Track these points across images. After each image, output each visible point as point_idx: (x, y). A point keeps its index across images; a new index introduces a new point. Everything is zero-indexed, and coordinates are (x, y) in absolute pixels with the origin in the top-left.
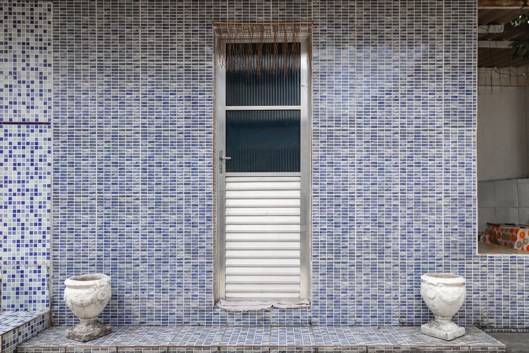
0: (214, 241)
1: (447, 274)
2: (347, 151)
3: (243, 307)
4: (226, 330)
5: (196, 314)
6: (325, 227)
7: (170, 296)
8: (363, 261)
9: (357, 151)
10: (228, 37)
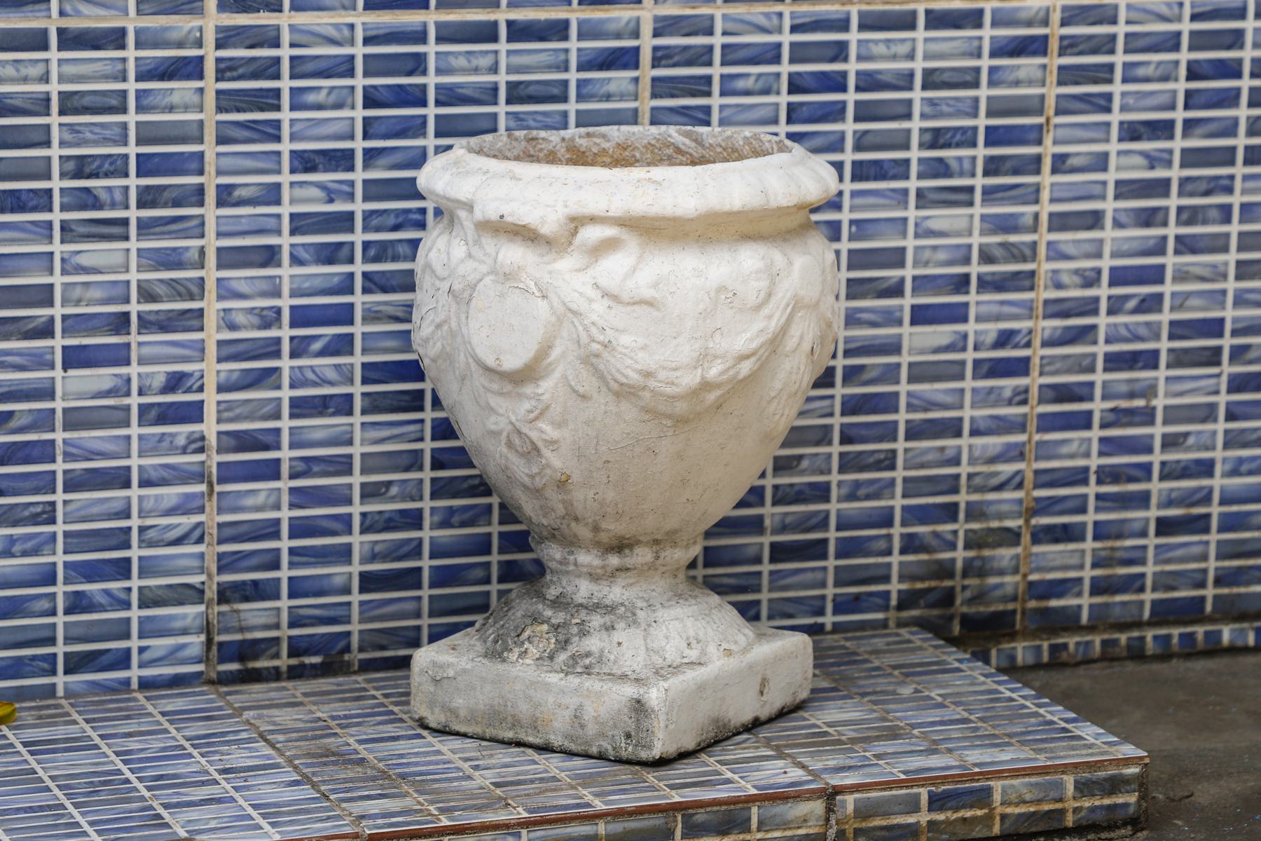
1: (673, 133)
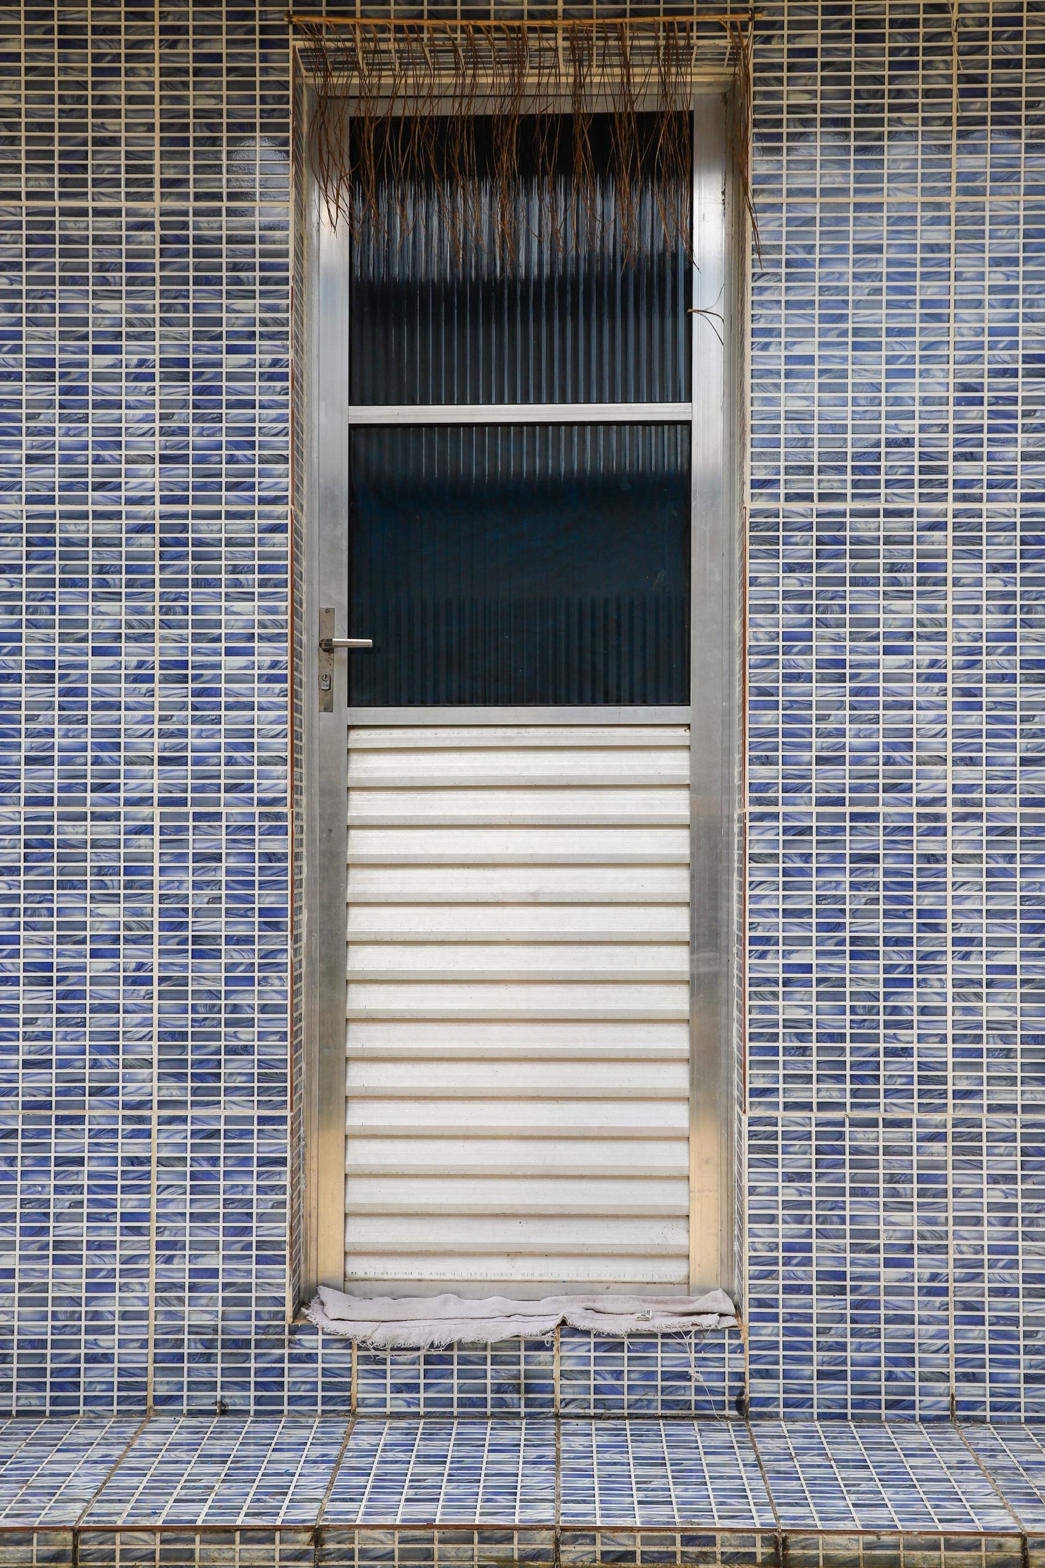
0: (295, 1021)
2: (908, 609)
3: (427, 1325)
4: (348, 1434)
5: (208, 1358)
6: (807, 956)
7: (92, 1273)
8: (984, 1116)
9: (957, 609)
10: (361, 86)
